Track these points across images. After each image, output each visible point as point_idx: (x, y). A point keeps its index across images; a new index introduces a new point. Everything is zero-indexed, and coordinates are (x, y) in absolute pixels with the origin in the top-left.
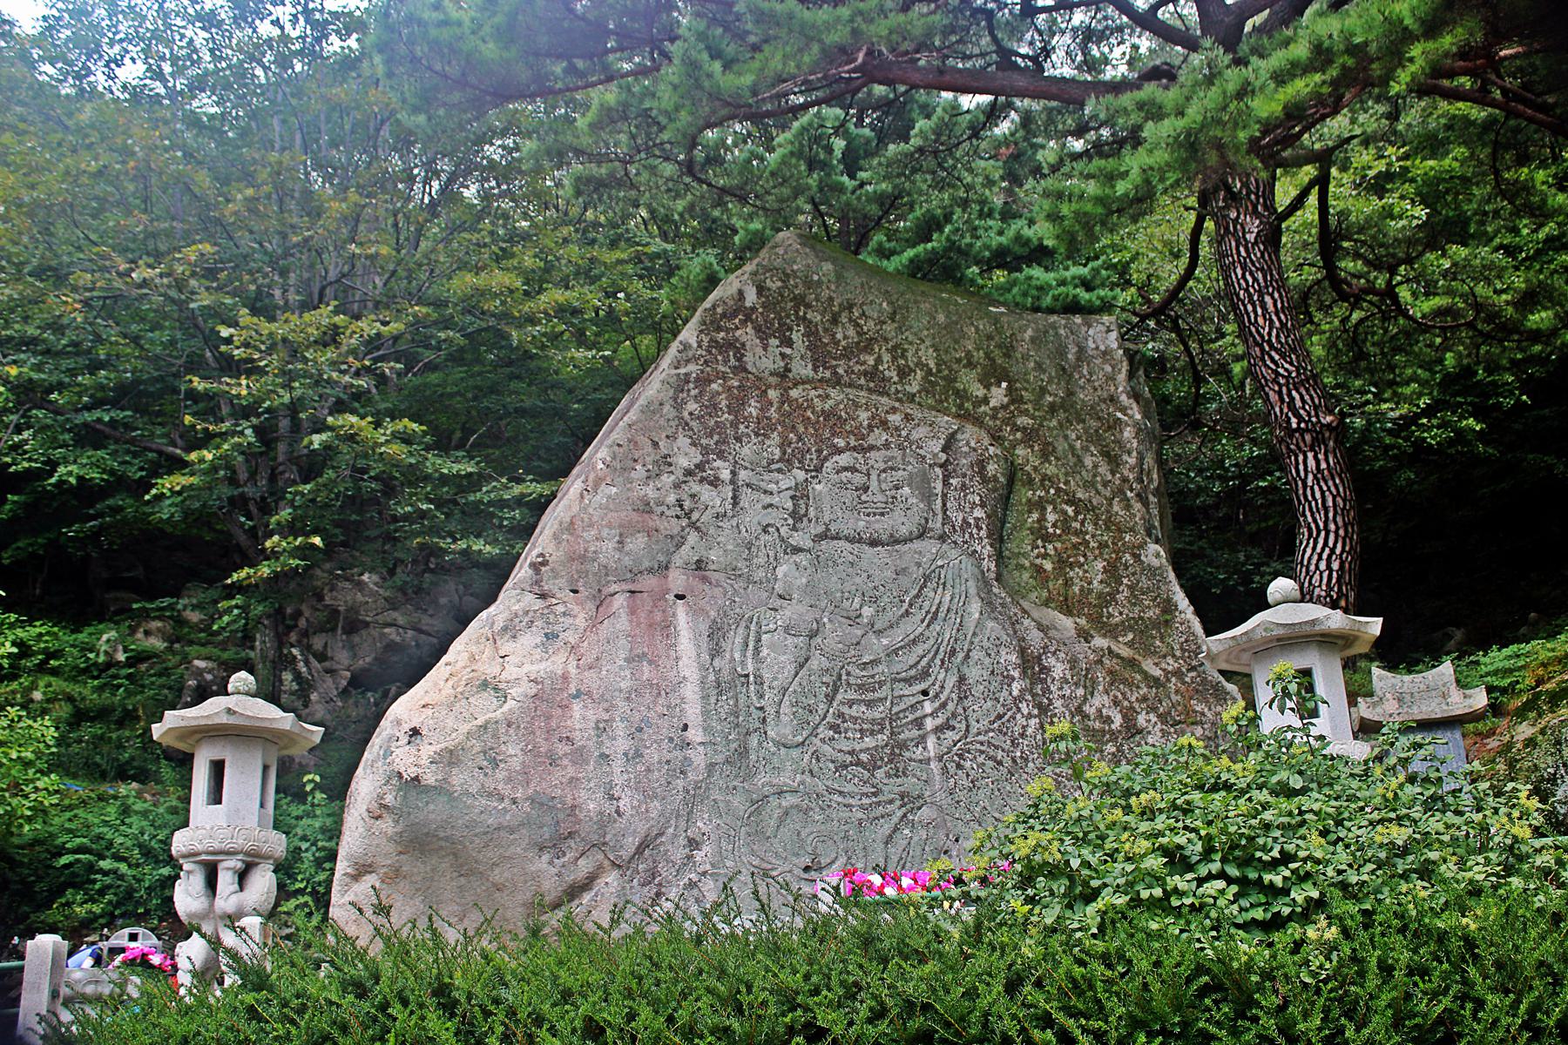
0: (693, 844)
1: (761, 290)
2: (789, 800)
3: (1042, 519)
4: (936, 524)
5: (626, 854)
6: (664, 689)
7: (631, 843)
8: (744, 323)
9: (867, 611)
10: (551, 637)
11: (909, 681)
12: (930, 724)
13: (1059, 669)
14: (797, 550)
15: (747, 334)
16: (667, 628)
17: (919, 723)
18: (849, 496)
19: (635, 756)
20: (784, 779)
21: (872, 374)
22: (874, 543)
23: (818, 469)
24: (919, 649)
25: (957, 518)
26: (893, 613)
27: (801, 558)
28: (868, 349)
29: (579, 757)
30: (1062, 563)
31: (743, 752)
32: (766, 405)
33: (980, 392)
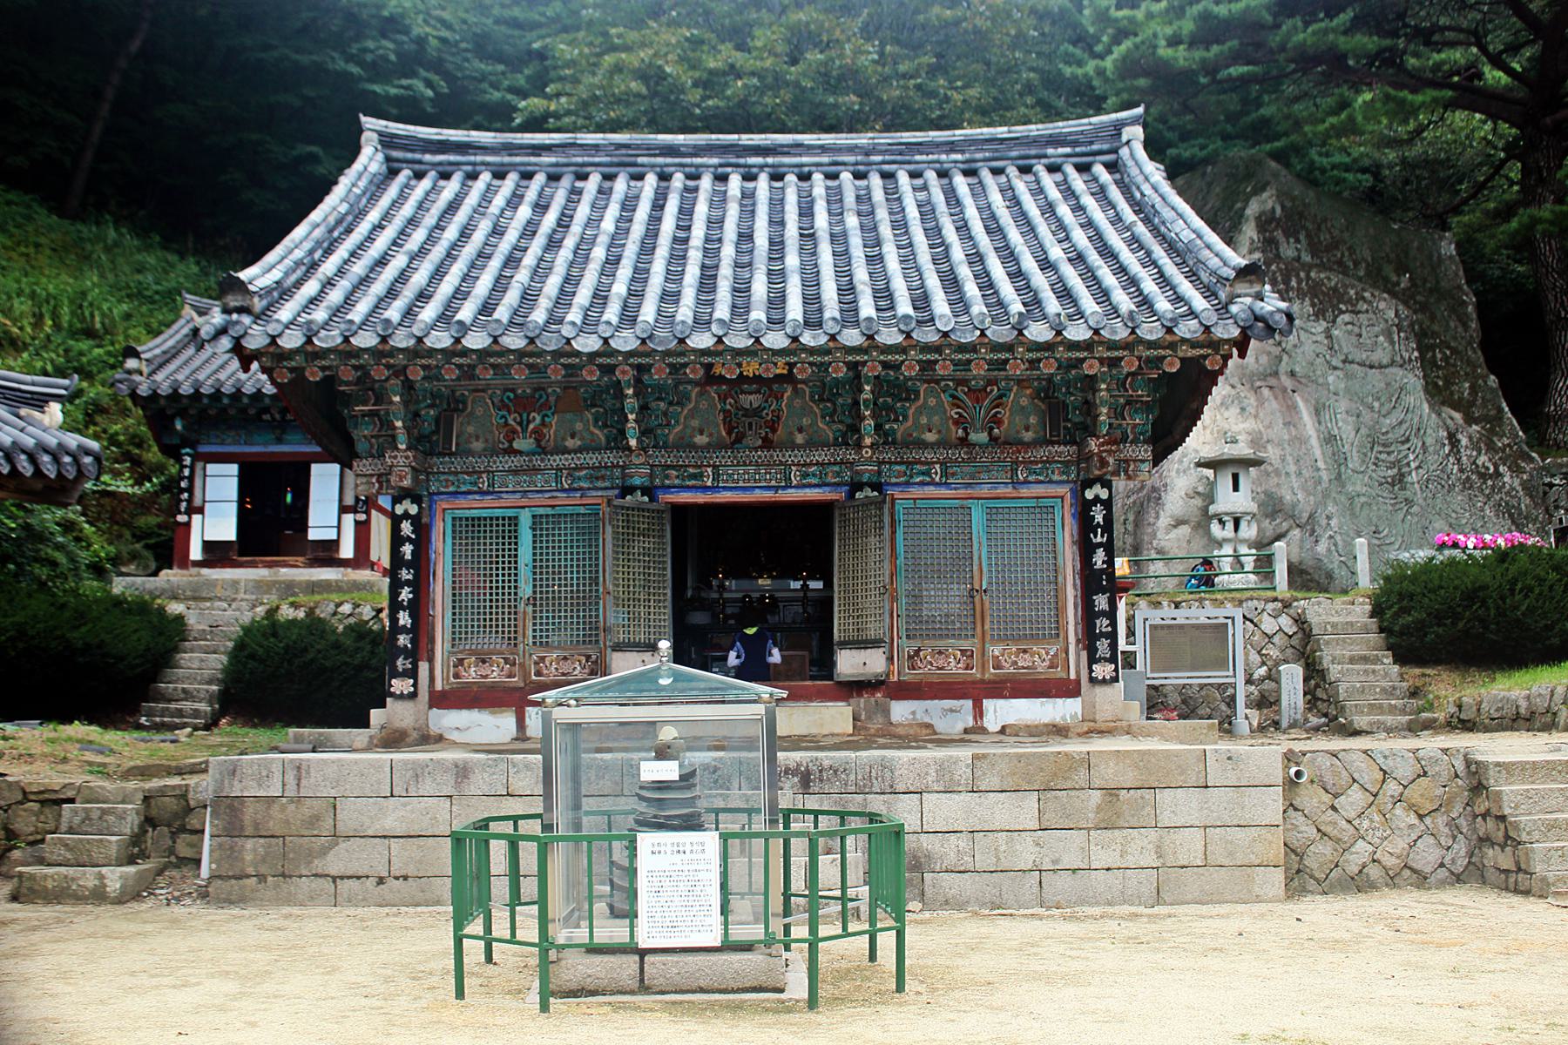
0: (1328, 518)
1: (1283, 207)
2: (1363, 499)
3: (1434, 356)
4: (1398, 358)
5: (1304, 521)
6: (1301, 440)
7: (1305, 515)
8: (1276, 228)
9: (1376, 404)
10: (1243, 409)
11: (1403, 443)
12: (1413, 465)
13: (1464, 441)
14: (1335, 368)
15: (1279, 234)
16: (1293, 408)
17: (1408, 464)
18: (1354, 339)
19: (1299, 474)
20: (1358, 488)
21: (1340, 263)
22: (1371, 367)
23: (1334, 322)
24: (1404, 426)
25: (1406, 355)
26: (1388, 406)
27: (1338, 373)
28: (1337, 248)
29: (1277, 472)
30: (1448, 383)
31: (1339, 474)
32: (1299, 282)
33: (1395, 279)
